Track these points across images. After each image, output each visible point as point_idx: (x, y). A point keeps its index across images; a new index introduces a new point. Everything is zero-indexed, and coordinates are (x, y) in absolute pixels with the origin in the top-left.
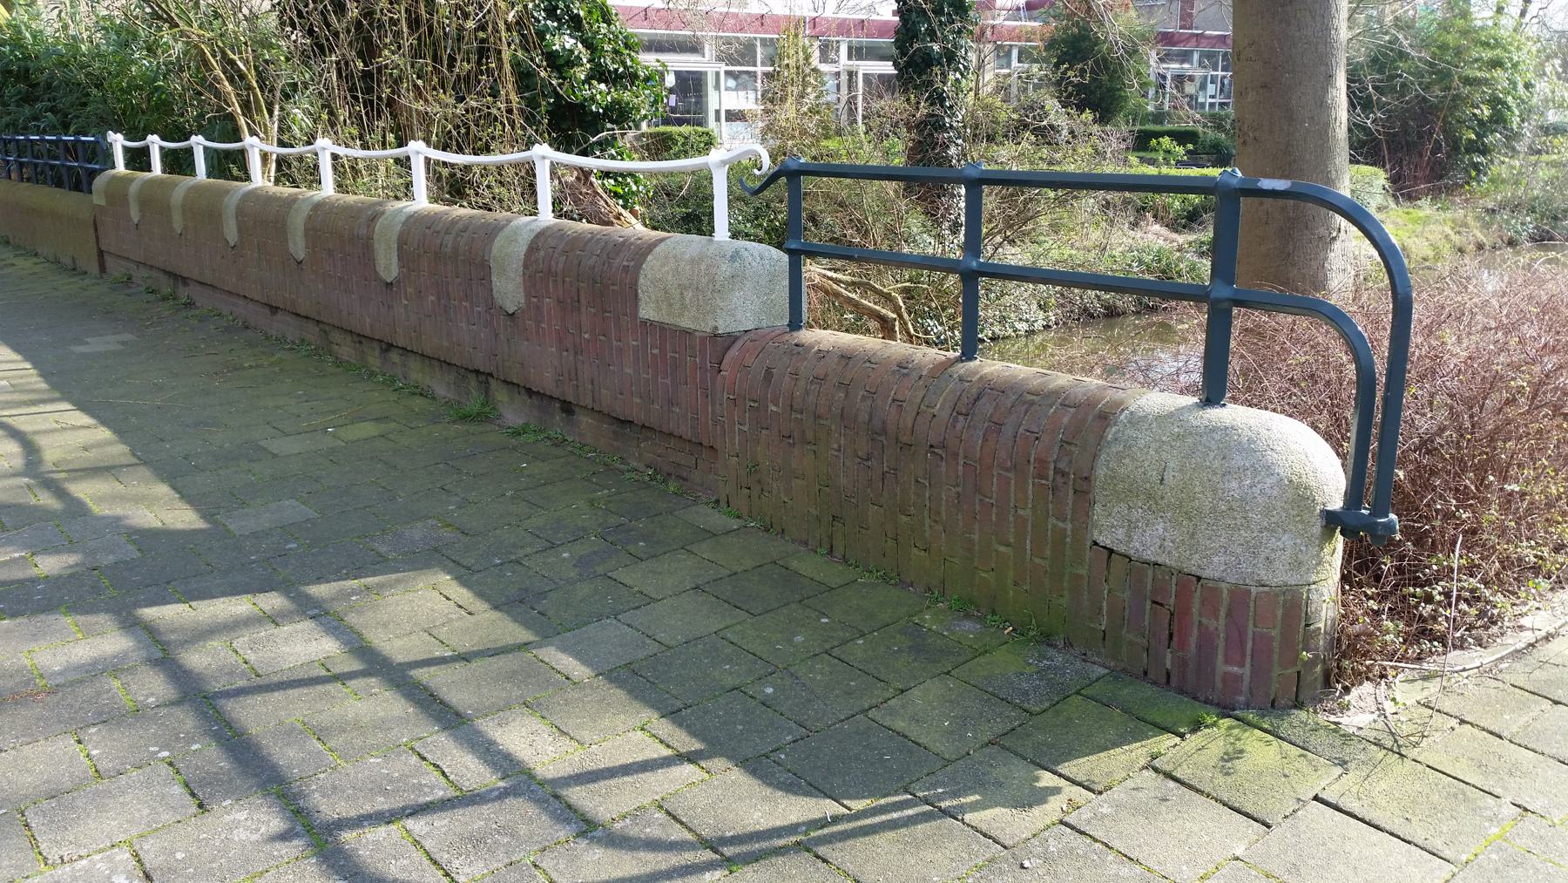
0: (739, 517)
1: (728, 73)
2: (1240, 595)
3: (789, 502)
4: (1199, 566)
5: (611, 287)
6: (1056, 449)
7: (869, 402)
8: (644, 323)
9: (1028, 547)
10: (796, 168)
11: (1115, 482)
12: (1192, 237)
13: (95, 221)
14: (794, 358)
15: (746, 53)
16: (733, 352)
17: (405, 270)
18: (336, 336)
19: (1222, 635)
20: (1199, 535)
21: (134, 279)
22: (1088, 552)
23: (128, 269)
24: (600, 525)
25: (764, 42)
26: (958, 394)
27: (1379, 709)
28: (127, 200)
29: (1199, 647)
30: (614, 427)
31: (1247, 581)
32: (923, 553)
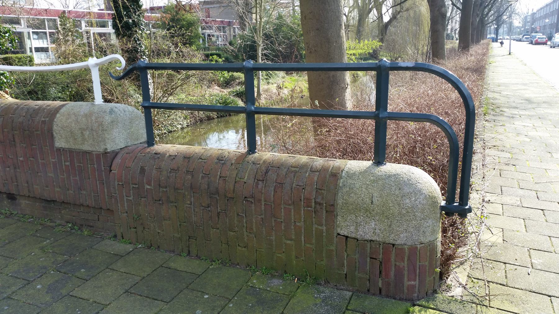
0: (130, 243)
1: (33, 32)
2: (413, 250)
3: (162, 232)
4: (394, 240)
5: (35, 133)
6: (314, 193)
7: (206, 179)
8: (59, 150)
9: (303, 240)
10: (145, 66)
11: (348, 205)
12: (229, 90)
14: (157, 160)
15: (41, 24)
16: (118, 160)
19: (406, 269)
20: (393, 226)
22: (335, 239)
24: (53, 263)
25: (49, 20)
26: (255, 171)
27: (460, 285)
29: (395, 276)
30: (43, 204)
31: (416, 243)
32: (244, 249)
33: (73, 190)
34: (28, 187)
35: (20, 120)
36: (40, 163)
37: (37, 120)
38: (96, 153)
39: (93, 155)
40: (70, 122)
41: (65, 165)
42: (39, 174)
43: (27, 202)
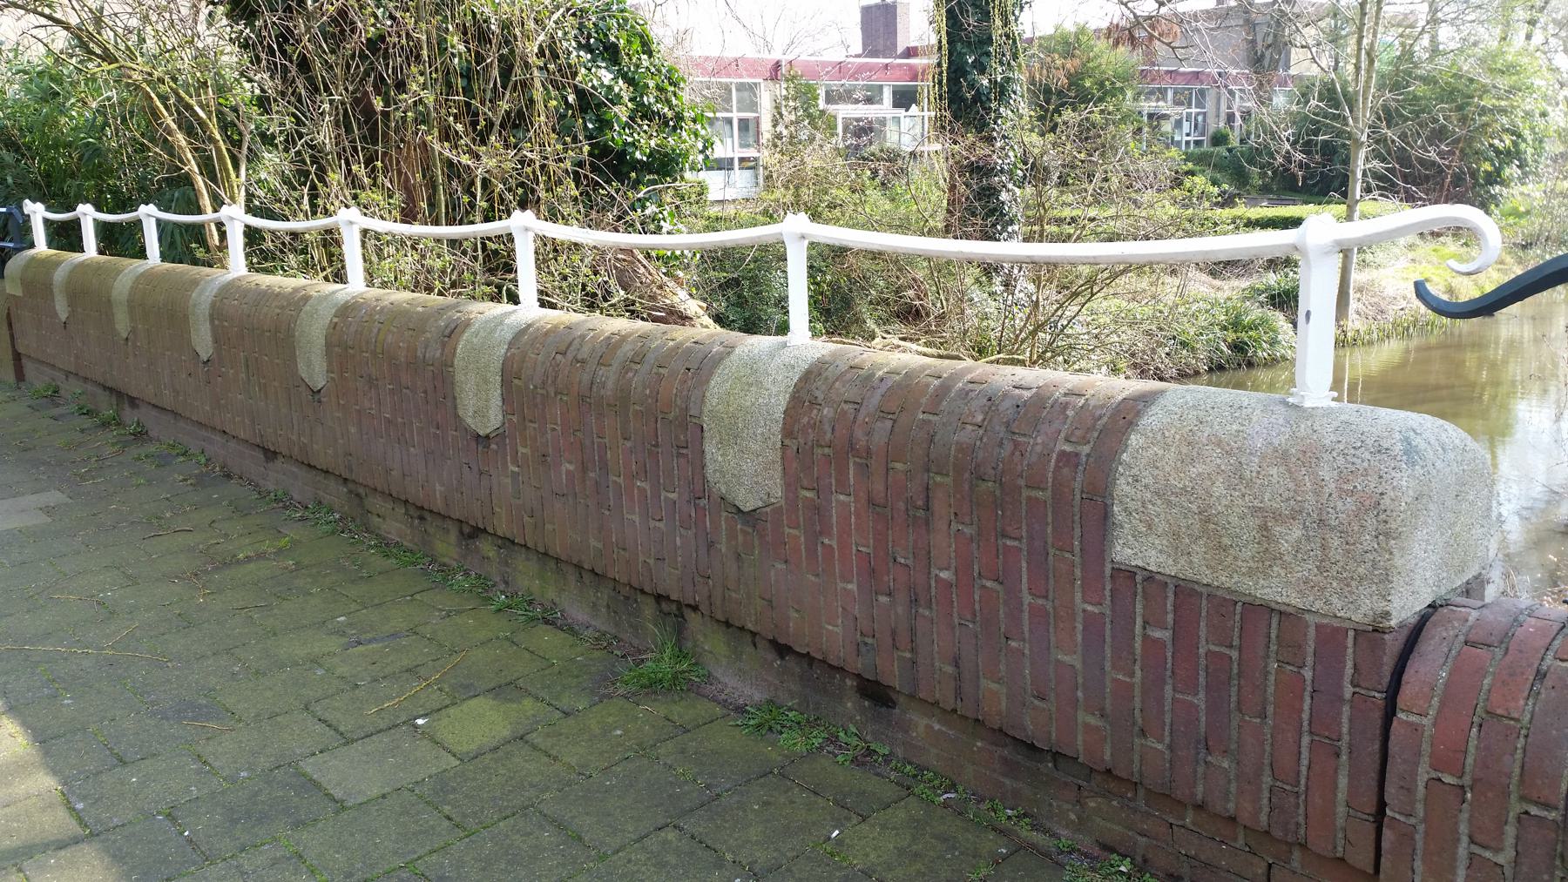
8: (1126, 575)
13: (8, 314)
17: (515, 419)
18: (377, 503)
21: (62, 392)
23: (54, 380)
28: (52, 291)
33: (1167, 740)
34: (958, 678)
35: (967, 435)
36: (1026, 607)
37: (1039, 449)
38: (1318, 620)
39: (1307, 626)
40: (1199, 474)
41: (1145, 637)
42: (1013, 644)
43: (937, 727)
